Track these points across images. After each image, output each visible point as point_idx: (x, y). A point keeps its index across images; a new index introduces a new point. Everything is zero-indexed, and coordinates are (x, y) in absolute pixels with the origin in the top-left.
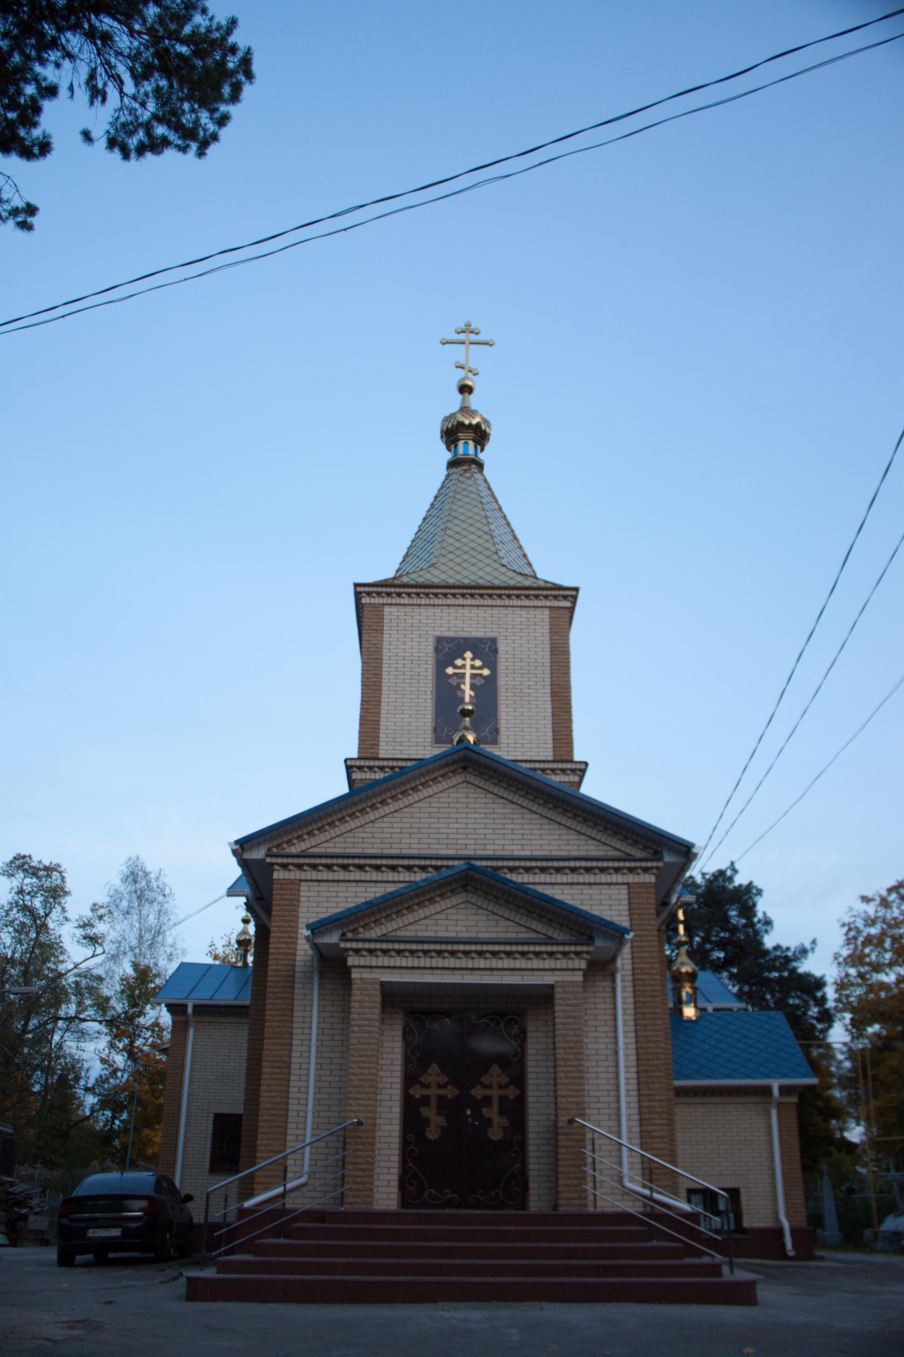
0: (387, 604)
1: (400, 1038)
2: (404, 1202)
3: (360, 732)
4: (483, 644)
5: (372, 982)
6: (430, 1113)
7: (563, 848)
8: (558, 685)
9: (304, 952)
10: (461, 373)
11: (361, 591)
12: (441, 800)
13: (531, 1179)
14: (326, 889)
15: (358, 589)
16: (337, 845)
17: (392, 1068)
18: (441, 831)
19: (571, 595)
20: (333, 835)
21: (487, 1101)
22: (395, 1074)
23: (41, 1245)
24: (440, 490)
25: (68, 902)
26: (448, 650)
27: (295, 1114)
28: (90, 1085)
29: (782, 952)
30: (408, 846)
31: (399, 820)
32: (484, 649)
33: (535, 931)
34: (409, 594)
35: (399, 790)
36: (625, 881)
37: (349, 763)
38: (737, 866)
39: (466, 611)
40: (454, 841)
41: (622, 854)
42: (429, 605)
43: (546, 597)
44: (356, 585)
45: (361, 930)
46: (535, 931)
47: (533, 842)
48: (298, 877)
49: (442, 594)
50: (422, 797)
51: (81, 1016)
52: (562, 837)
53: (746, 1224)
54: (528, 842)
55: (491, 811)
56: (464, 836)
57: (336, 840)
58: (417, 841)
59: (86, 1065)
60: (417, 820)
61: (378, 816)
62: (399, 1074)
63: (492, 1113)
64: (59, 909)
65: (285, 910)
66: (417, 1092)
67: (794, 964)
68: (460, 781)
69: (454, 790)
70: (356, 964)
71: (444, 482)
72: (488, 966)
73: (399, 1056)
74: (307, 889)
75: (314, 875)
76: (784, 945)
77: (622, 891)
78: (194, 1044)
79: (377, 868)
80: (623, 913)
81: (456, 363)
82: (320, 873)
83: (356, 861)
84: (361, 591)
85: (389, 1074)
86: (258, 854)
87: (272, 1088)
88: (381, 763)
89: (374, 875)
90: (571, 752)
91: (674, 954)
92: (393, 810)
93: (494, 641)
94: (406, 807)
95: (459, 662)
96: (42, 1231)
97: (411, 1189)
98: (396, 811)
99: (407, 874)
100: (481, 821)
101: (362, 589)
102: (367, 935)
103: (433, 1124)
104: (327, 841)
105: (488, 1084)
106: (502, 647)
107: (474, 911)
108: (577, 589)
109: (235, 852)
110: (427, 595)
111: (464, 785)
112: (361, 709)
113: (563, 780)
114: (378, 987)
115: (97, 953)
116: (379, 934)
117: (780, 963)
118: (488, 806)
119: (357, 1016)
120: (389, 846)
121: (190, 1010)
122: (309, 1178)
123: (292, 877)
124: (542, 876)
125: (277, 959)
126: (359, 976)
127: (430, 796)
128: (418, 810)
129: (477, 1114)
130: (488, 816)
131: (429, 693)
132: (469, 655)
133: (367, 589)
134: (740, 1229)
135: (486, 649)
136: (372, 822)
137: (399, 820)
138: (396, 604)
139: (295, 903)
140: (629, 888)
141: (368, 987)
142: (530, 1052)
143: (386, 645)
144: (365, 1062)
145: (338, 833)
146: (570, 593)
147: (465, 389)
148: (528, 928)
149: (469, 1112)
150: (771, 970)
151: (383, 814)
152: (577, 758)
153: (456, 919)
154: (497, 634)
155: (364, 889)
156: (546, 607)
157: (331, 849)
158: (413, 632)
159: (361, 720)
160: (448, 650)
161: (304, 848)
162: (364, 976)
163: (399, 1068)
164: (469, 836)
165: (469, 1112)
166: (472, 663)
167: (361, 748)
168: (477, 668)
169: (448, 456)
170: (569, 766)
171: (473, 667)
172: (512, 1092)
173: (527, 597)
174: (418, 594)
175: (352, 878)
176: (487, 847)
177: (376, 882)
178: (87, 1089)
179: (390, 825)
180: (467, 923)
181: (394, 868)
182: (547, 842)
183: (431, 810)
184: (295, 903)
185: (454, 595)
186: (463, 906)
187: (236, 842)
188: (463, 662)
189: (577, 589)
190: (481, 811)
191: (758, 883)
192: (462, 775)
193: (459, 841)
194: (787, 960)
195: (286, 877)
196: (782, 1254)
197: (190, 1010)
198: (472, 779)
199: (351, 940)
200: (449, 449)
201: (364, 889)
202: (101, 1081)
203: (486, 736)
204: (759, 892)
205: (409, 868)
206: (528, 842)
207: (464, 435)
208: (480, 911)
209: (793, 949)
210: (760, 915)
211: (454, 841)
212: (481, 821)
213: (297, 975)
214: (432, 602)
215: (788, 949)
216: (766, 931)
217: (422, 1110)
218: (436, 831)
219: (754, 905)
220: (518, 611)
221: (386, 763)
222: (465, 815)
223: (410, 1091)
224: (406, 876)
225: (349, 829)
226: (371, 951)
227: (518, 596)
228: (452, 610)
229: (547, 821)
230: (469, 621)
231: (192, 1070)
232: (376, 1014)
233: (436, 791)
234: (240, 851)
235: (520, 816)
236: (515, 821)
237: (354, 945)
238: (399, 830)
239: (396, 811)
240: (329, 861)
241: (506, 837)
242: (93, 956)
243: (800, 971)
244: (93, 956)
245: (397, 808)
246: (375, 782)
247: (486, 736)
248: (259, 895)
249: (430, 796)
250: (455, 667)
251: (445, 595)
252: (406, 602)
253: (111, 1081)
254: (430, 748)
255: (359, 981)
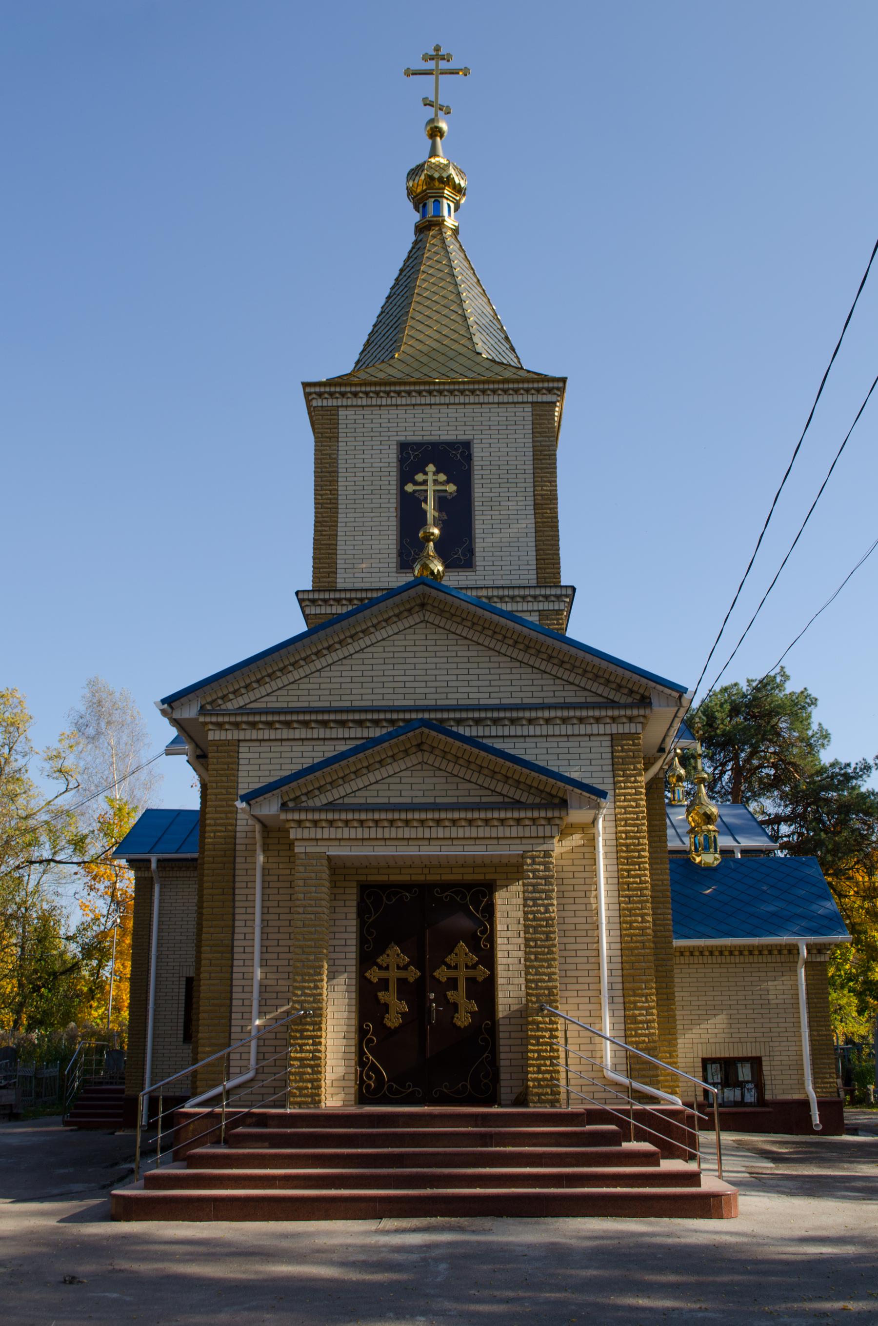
0: (342, 406)
1: (354, 916)
2: (362, 1098)
3: (314, 559)
4: (455, 450)
5: (319, 856)
6: (390, 997)
7: (535, 694)
8: (542, 495)
9: (245, 822)
10: (430, 112)
11: (313, 391)
12: (396, 643)
13: (502, 1070)
14: (268, 749)
15: (308, 390)
16: (280, 699)
17: (347, 949)
18: (396, 679)
19: (556, 386)
20: (275, 688)
21: (453, 983)
22: (349, 956)
23: (10, 1120)
24: (406, 261)
25: (32, 732)
26: (413, 457)
27: (240, 1002)
28: (70, 934)
29: (841, 769)
30: (359, 697)
31: (349, 668)
32: (456, 455)
33: (501, 794)
34: (367, 394)
35: (348, 634)
36: (608, 732)
37: (301, 596)
38: (788, 671)
39: (434, 411)
40: (412, 691)
41: (605, 700)
42: (391, 405)
43: (527, 391)
44: (305, 385)
45: (304, 798)
46: (501, 794)
47: (502, 689)
48: (236, 737)
49: (405, 391)
50: (374, 641)
51: (57, 858)
52: (535, 682)
53: (768, 1097)
54: (497, 689)
55: (454, 654)
56: (423, 684)
57: (278, 693)
58: (370, 691)
59: (65, 912)
60: (370, 667)
61: (325, 664)
62: (354, 955)
63: (459, 996)
64: (22, 738)
65: (222, 775)
66: (374, 975)
67: (854, 782)
68: (418, 620)
69: (411, 631)
70: (299, 836)
71: (410, 252)
72: (447, 835)
73: (354, 936)
74: (247, 749)
75: (254, 734)
76: (843, 761)
77: (604, 744)
78: (160, 902)
79: (325, 724)
80: (605, 768)
81: (424, 99)
82: (261, 732)
83: (301, 717)
84: (313, 391)
85: (343, 955)
86: (190, 712)
87: (213, 975)
88: (337, 595)
89: (322, 733)
90: (557, 574)
91: (717, 772)
92: (341, 656)
93: (467, 446)
94: (356, 652)
95: (420, 477)
96: (11, 1105)
97: (368, 1082)
98: (345, 658)
99: (359, 730)
100: (443, 666)
101: (312, 390)
102: (311, 803)
103: (392, 1010)
104: (268, 695)
105: (453, 964)
106: (478, 453)
107: (431, 773)
108: (564, 380)
109: (164, 713)
110: (388, 393)
111: (423, 625)
112: (315, 531)
113: (546, 608)
114: (325, 862)
115: (70, 786)
116: (325, 802)
117: (839, 780)
118: (450, 648)
119: (301, 896)
120: (338, 698)
121: (154, 865)
122: (257, 1073)
123: (229, 737)
124: (513, 728)
125: (215, 832)
126: (302, 850)
127: (383, 639)
128: (370, 656)
129: (442, 999)
130: (450, 660)
131: (392, 510)
132: (431, 468)
133: (317, 389)
134: (761, 1101)
135: (455, 459)
136: (318, 671)
137: (349, 668)
138: (352, 406)
139: (234, 767)
140: (612, 740)
141: (314, 862)
142: (499, 927)
143: (342, 455)
144: (312, 947)
145: (280, 685)
146: (556, 385)
147: (435, 132)
148: (492, 791)
149: (432, 996)
150: (827, 788)
151: (330, 661)
152: (563, 583)
153: (406, 782)
154: (471, 437)
155: (310, 748)
156: (527, 403)
157: (272, 703)
158: (375, 439)
159: (314, 544)
160: (413, 457)
161: (242, 704)
162: (309, 850)
163: (354, 949)
164: (429, 684)
165: (432, 996)
166: (435, 478)
167: (316, 578)
168: (442, 484)
169: (416, 217)
170: (554, 591)
171: (436, 482)
172: (482, 972)
173: (505, 391)
174: (377, 393)
175: (297, 736)
176: (450, 696)
177: (324, 739)
178: (68, 938)
179: (339, 674)
180: (424, 787)
181: (343, 723)
182: (518, 689)
183: (385, 655)
184: (234, 767)
185: (420, 393)
186: (419, 767)
187: (163, 701)
188: (425, 477)
189: (564, 380)
190: (442, 654)
191: (813, 692)
192: (420, 614)
193: (417, 691)
194: (848, 778)
195: (223, 738)
196: (805, 1127)
197: (154, 865)
198: (431, 618)
199: (293, 810)
200: (417, 209)
201: (310, 748)
202: (84, 928)
203: (459, 558)
204: (814, 702)
205: (360, 723)
206: (497, 689)
207: (427, 190)
208: (438, 773)
209: (853, 766)
210: (815, 727)
211: (412, 691)
212: (443, 666)
213: (238, 847)
214: (394, 402)
215: (848, 765)
216: (823, 745)
217: (380, 994)
218: (391, 679)
219: (809, 716)
220: (495, 409)
221: (343, 595)
222: (424, 660)
223: (367, 974)
224: (358, 732)
225: (292, 680)
226: (315, 823)
227: (494, 391)
228: (418, 410)
229: (518, 664)
230: (437, 424)
231: (160, 930)
232: (325, 889)
233: (391, 633)
234: (169, 710)
235: (487, 659)
236: (481, 665)
237: (296, 816)
238: (349, 680)
239: (345, 658)
240: (270, 718)
241: (471, 683)
242: (66, 791)
243: (863, 790)
244: (66, 791)
245: (347, 654)
246: (335, 615)
247: (459, 558)
248: (199, 752)
249: (383, 639)
250: (416, 483)
251: (409, 393)
252: (364, 403)
253: (95, 928)
254: (394, 574)
255: (303, 856)
